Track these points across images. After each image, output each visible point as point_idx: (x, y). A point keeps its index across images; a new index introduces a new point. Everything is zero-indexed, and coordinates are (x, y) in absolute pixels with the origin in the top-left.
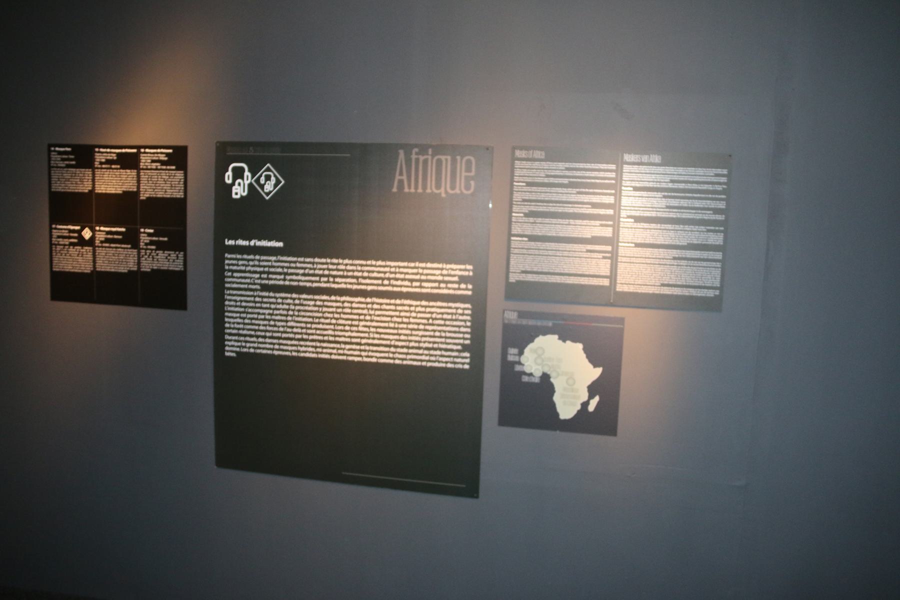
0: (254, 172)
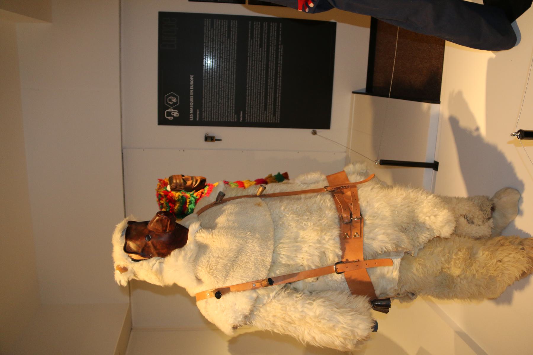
0: (168, 108)
